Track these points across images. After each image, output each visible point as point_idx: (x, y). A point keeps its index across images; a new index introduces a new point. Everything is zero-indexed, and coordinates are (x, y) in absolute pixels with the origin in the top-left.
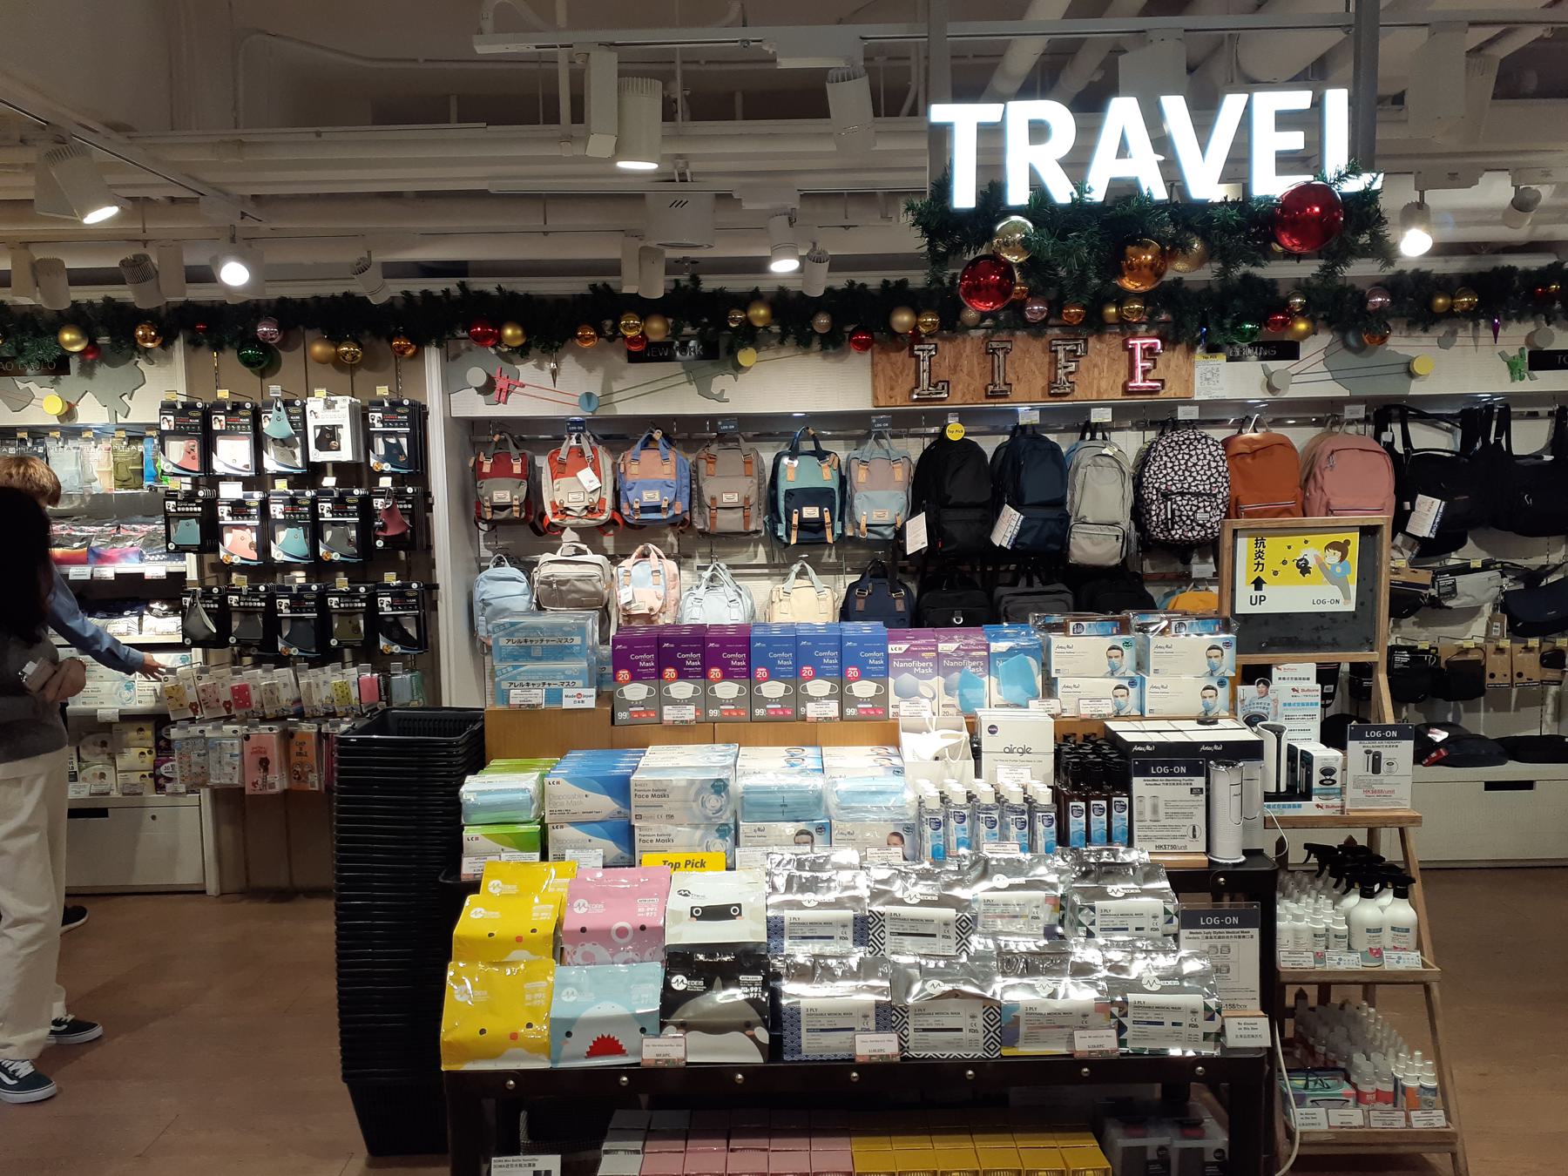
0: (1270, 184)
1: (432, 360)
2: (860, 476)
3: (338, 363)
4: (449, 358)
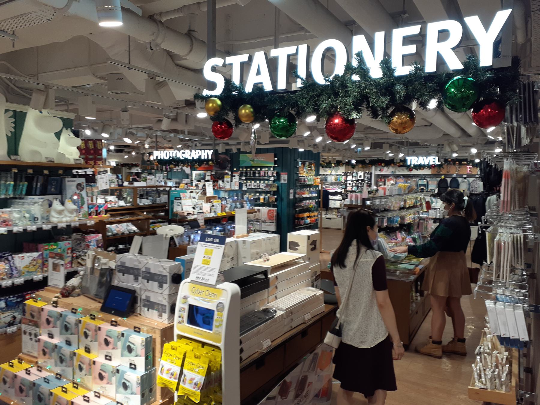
0: (402, 70)
1: (373, 167)
2: (430, 183)
3: (362, 167)
4: (376, 167)
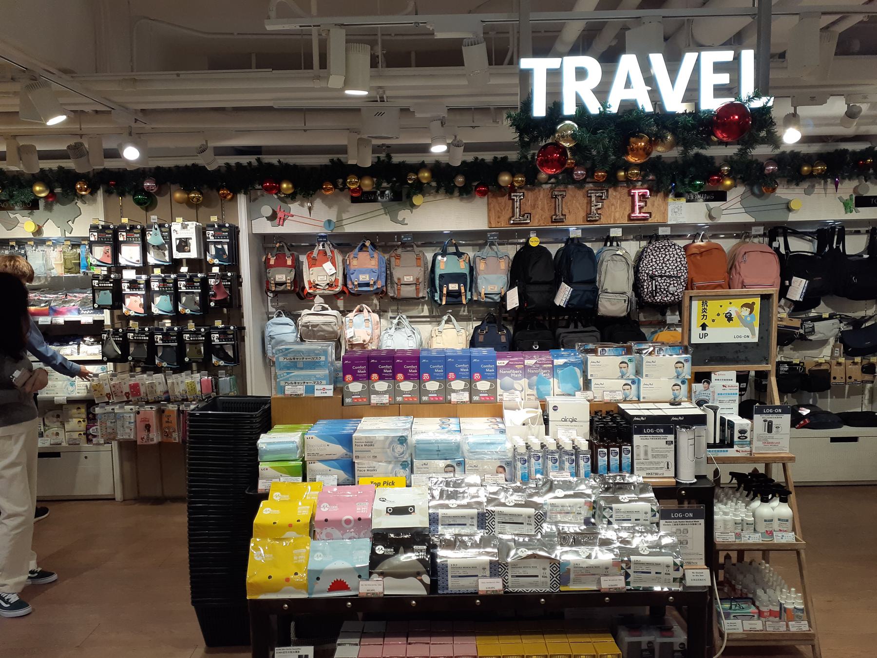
1: (242, 201)
2: (481, 266)
3: (189, 203)
4: (251, 200)
